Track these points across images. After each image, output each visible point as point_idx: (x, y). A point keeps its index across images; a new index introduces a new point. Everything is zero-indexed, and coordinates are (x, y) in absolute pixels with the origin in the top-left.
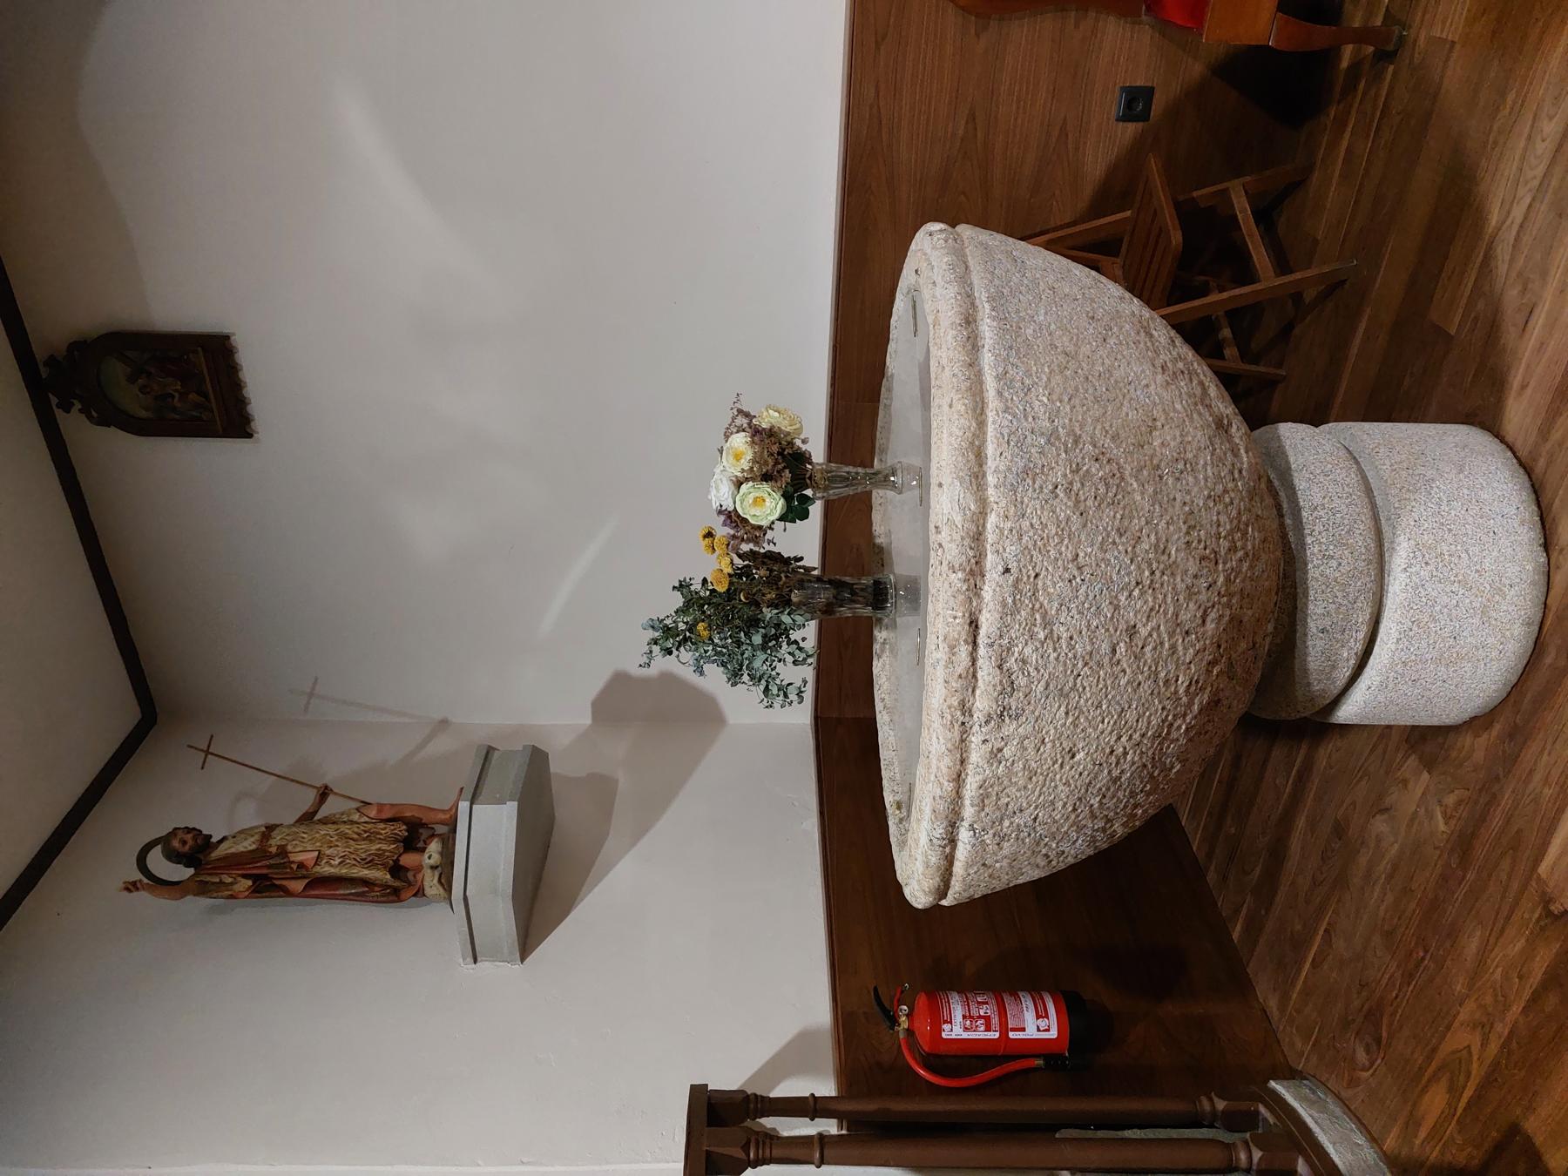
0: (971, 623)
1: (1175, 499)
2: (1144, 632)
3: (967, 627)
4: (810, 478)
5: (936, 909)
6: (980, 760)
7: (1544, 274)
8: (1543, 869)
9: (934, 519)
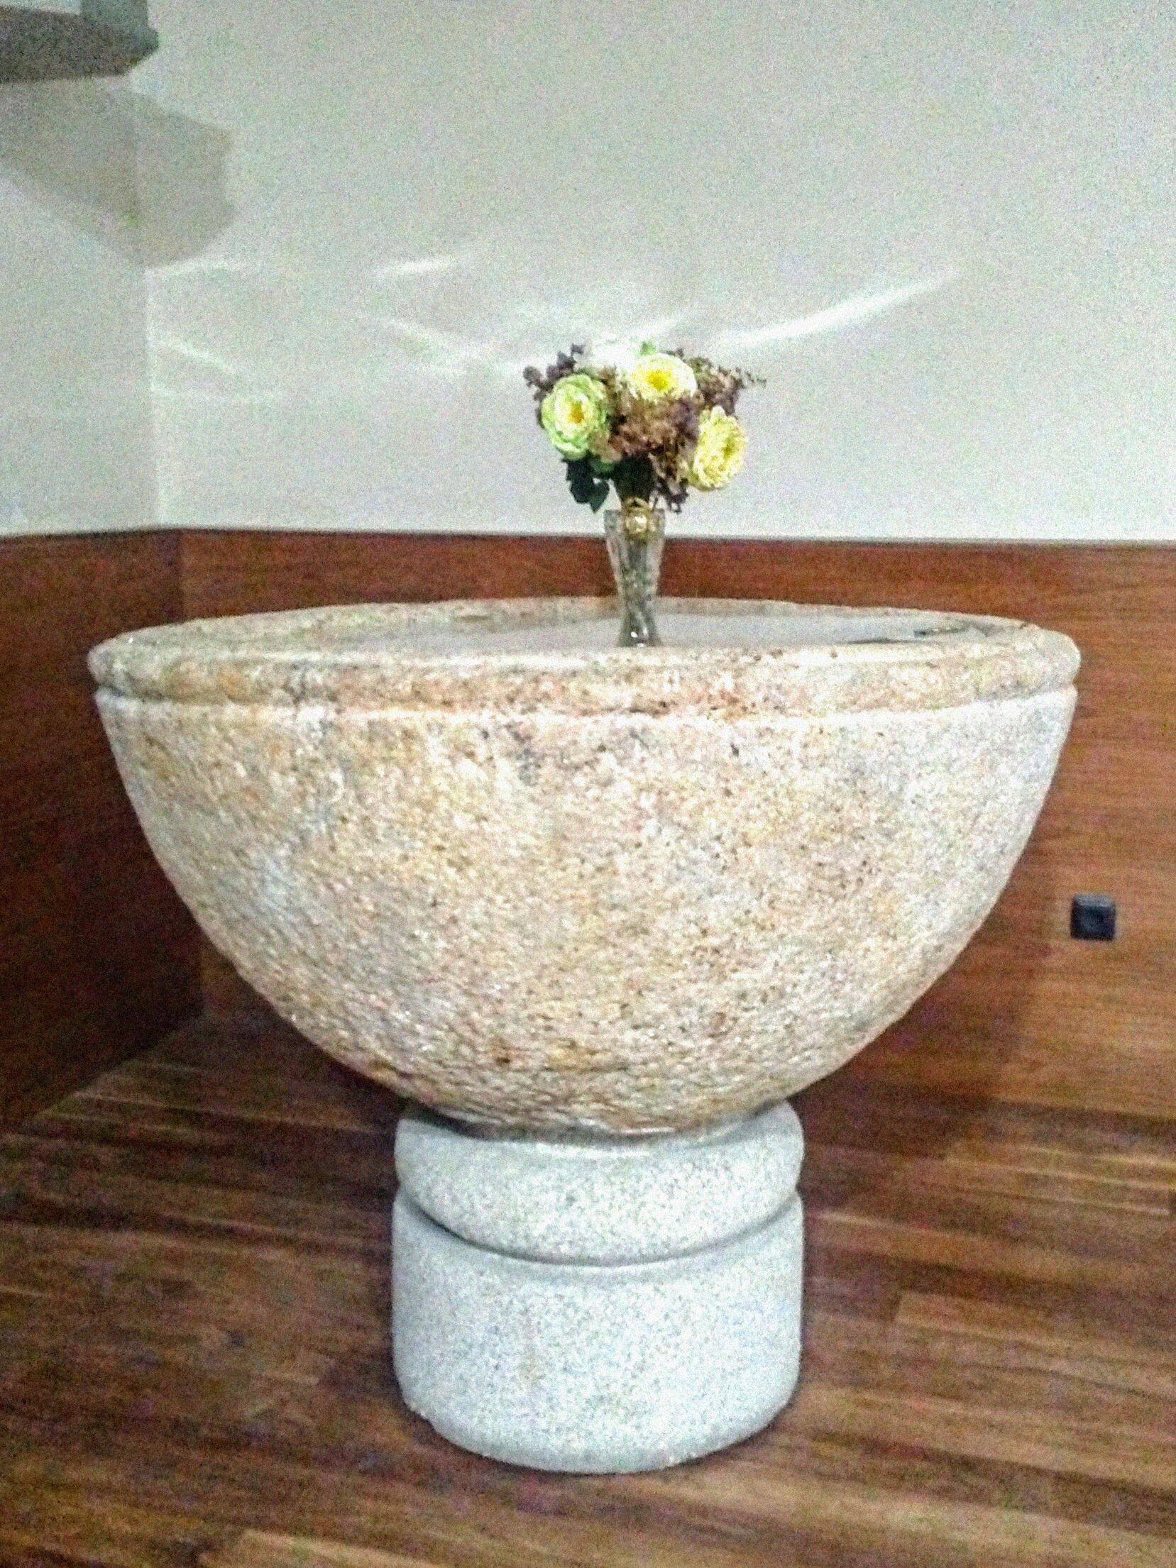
0: (664, 704)
1: (802, 972)
2: (636, 945)
3: (657, 698)
4: (636, 504)
5: (89, 684)
6: (453, 728)
7: (1003, 1404)
8: (250, 1533)
9: (840, 650)
